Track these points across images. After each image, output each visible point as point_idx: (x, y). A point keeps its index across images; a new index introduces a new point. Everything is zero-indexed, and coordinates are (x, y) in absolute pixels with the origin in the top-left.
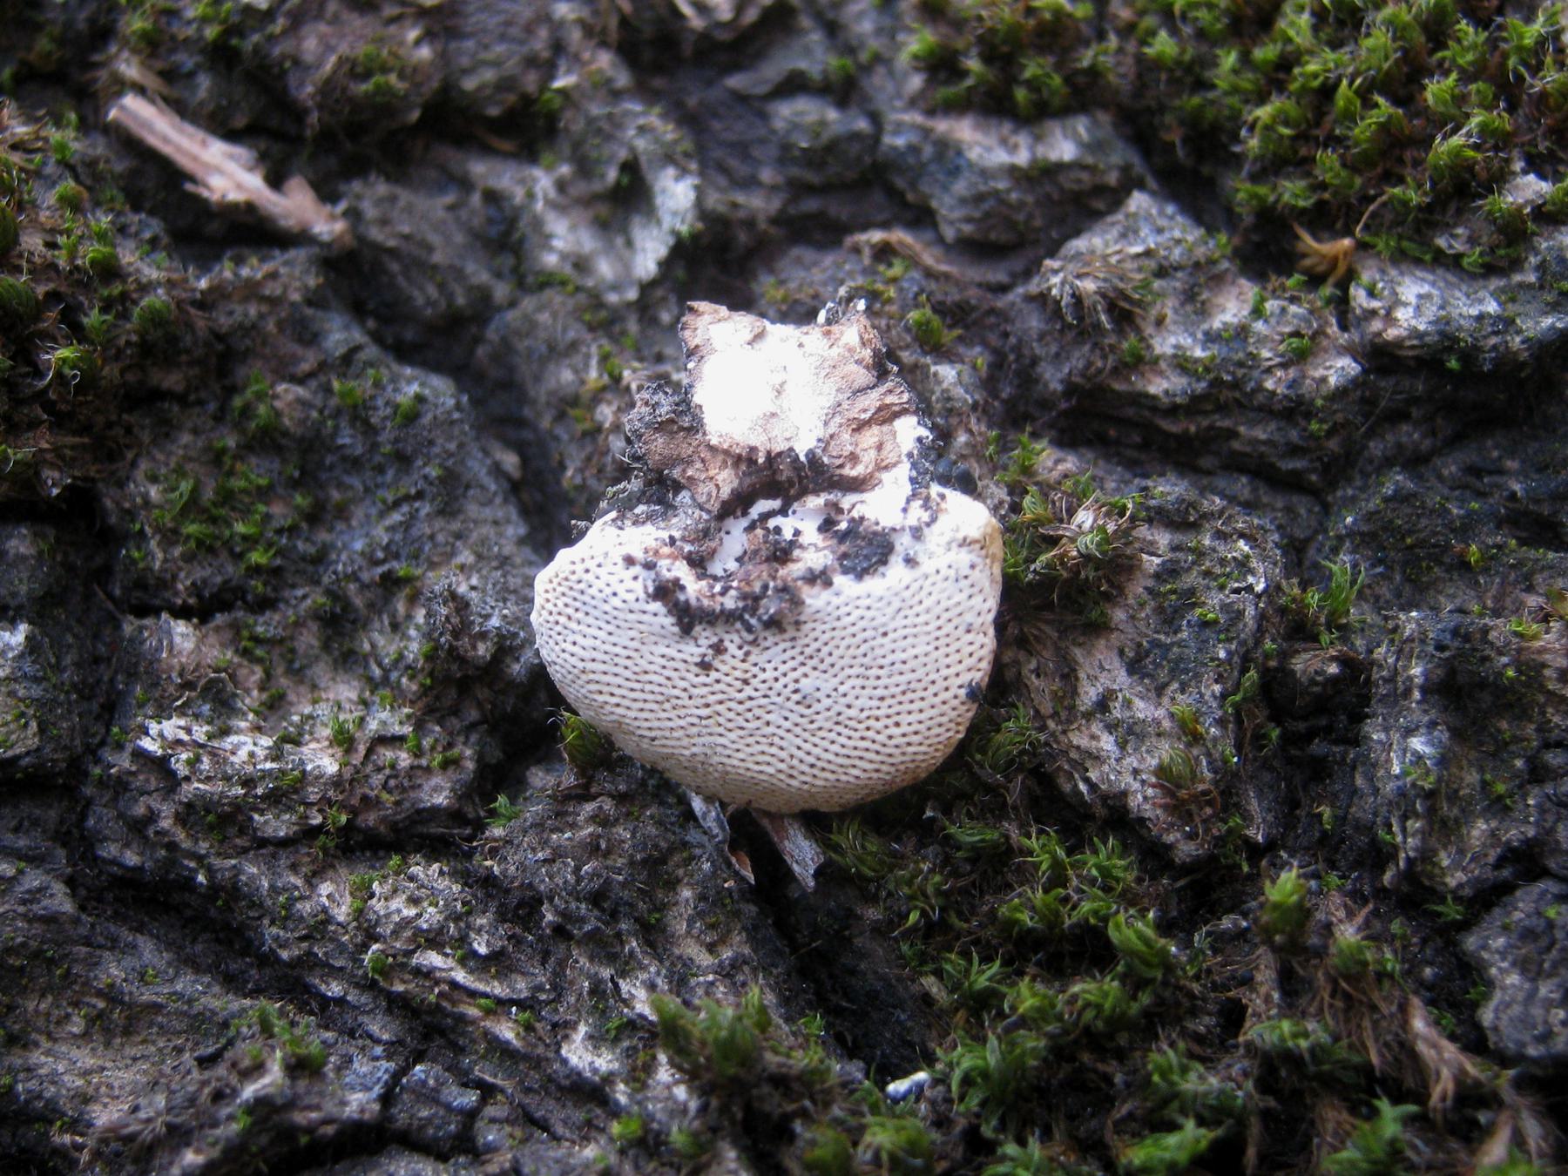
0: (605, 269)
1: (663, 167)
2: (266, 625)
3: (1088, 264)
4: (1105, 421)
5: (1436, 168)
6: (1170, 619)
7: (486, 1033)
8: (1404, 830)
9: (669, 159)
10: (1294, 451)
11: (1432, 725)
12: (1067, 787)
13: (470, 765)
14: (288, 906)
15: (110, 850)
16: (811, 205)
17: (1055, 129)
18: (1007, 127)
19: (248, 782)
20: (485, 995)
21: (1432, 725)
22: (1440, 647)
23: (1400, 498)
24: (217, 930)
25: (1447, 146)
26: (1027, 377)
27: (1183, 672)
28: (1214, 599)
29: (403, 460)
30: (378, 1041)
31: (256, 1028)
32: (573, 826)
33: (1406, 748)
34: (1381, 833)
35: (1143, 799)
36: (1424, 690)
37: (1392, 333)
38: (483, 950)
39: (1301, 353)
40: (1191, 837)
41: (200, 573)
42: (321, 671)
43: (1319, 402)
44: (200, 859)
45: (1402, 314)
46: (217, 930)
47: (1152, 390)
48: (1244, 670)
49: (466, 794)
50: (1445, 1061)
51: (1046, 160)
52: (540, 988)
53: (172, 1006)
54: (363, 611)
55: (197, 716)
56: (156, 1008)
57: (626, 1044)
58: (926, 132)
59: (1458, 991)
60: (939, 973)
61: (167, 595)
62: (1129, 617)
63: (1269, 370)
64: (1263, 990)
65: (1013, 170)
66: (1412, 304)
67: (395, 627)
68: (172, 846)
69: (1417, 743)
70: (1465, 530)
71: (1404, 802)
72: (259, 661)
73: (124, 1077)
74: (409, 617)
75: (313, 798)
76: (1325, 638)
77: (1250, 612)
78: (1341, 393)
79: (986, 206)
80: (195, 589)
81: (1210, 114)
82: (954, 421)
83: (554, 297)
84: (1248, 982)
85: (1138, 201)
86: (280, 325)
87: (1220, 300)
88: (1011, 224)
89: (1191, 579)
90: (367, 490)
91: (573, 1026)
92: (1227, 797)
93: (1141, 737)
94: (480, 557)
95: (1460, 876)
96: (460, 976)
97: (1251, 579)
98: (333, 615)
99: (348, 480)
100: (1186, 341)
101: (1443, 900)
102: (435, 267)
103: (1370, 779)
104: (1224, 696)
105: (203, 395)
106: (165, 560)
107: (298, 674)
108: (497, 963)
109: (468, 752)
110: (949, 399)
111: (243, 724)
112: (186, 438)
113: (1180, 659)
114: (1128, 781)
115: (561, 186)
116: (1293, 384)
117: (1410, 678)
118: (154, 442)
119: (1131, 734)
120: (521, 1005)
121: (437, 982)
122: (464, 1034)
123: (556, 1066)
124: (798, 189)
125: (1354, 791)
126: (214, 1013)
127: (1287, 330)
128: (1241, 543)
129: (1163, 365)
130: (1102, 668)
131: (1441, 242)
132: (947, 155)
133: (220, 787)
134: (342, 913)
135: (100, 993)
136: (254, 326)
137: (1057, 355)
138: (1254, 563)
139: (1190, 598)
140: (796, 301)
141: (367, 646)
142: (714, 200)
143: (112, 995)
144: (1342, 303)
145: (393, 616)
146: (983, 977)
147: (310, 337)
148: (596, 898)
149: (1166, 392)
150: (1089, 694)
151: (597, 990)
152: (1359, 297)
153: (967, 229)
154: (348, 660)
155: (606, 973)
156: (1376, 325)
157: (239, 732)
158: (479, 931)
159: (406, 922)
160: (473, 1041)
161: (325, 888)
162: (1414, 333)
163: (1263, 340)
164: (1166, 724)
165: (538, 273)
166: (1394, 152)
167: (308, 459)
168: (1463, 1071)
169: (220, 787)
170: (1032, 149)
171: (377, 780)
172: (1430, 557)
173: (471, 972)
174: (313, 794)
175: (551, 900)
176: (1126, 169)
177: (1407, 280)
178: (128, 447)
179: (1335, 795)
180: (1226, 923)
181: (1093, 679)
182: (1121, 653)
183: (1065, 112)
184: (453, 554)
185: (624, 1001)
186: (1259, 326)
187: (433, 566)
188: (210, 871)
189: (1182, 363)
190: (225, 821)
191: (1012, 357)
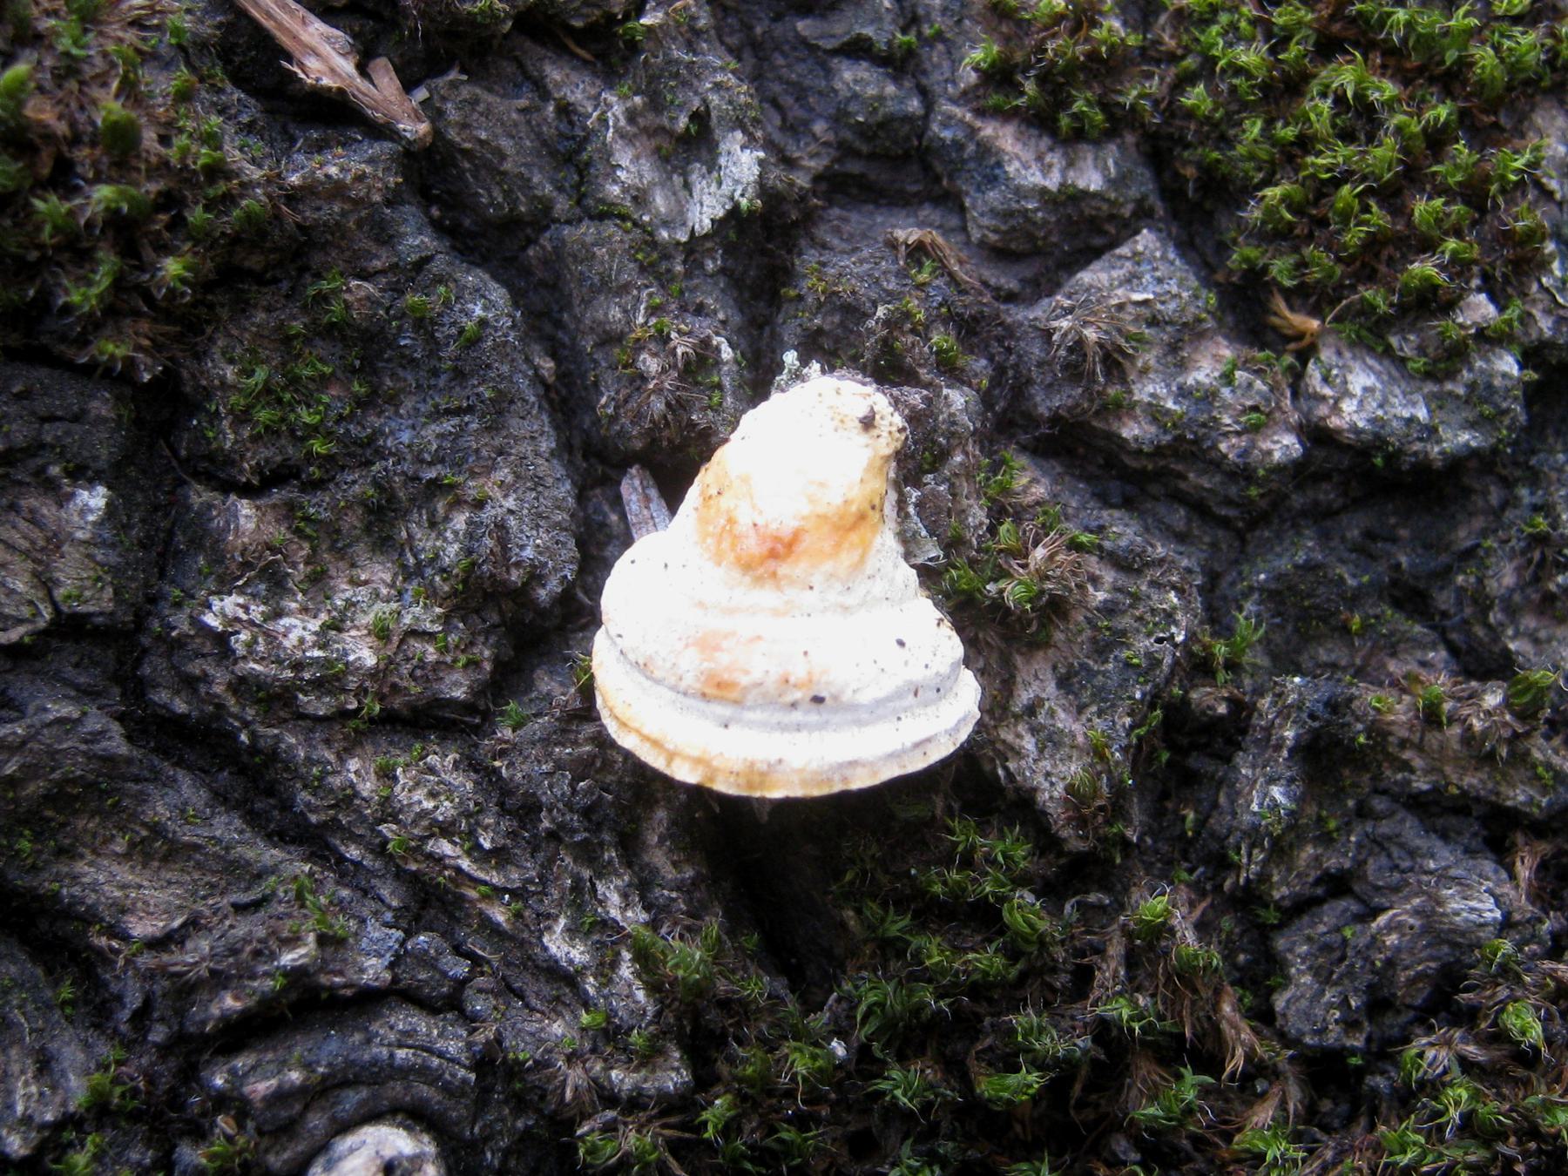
0: (660, 202)
1: (733, 129)
2: (317, 506)
3: (1094, 314)
4: (1081, 448)
5: (1406, 285)
6: (1102, 650)
7: (481, 913)
8: (1250, 855)
9: (739, 124)
10: (1228, 502)
11: (1291, 781)
12: (987, 767)
13: (488, 666)
14: (321, 779)
15: (162, 696)
16: (854, 167)
17: (1087, 154)
18: (1046, 142)
19: (298, 666)
20: (485, 883)
21: (1291, 781)
22: (1312, 716)
23: (1310, 567)
24: (261, 790)
25: (1423, 268)
26: (1020, 390)
27: (1105, 701)
28: (1143, 644)
29: (459, 375)
30: (389, 907)
31: (292, 895)
32: (575, 743)
33: (1265, 794)
34: (1232, 853)
35: (1050, 795)
36: (1291, 751)
37: (1334, 422)
38: (487, 845)
39: (1258, 422)
40: (1085, 838)
41: (264, 453)
42: (361, 550)
43: (1261, 472)
44: (246, 724)
45: (1348, 406)
46: (261, 790)
47: (1125, 433)
48: (1152, 707)
49: (478, 691)
50: (1242, 1040)
51: (1074, 186)
52: (530, 881)
53: (211, 849)
54: (406, 504)
55: (254, 596)
56: (197, 847)
57: (596, 937)
58: (972, 132)
59: (1260, 977)
60: (859, 911)
61: (234, 471)
62: (1071, 640)
63: (1226, 435)
64: (1113, 965)
65: (1044, 191)
66: (1360, 394)
67: (433, 524)
68: (220, 707)
69: (1277, 792)
70: (1354, 600)
71: (1254, 835)
72: (308, 538)
73: (157, 896)
74: (447, 519)
75: (352, 686)
76: (1222, 676)
77: (1168, 660)
78: (1279, 469)
79: (1013, 222)
80: (257, 470)
81: (1224, 169)
82: (954, 442)
83: (610, 229)
84: (1100, 951)
85: (1146, 240)
86: (360, 224)
87: (1197, 356)
88: (1031, 238)
89: (1125, 622)
90: (419, 386)
91: (556, 918)
92: (1117, 809)
93: (1057, 745)
94: (518, 476)
95: (1285, 890)
96: (465, 864)
97: (1173, 629)
98: (380, 507)
99: (401, 373)
100: (1161, 391)
101: (1267, 906)
102: (504, 173)
103: (1232, 802)
104: (1132, 727)
105: (278, 273)
106: (236, 442)
107: (341, 553)
108: (499, 857)
109: (487, 653)
110: (954, 423)
111: (294, 605)
112: (260, 317)
113: (1103, 688)
114: (1039, 780)
115: (632, 116)
116: (1245, 453)
117: (1283, 739)
118: (231, 319)
119: (1051, 741)
120: (515, 894)
121: (446, 867)
122: (461, 908)
123: (537, 950)
124: (845, 150)
125: (1215, 805)
126: (248, 863)
127: (1249, 403)
128: (1172, 594)
129: (1138, 411)
130: (1036, 677)
131: (1394, 341)
132: (989, 164)
133: (273, 670)
134: (367, 787)
135: (144, 825)
136: (337, 223)
137: (1050, 385)
138: (1179, 616)
139: (1120, 638)
140: (836, 293)
141: (404, 534)
142: (776, 175)
143: (157, 830)
144: (1297, 377)
145: (432, 514)
146: (896, 926)
147: (385, 236)
148: (587, 812)
149: (1136, 439)
150: (1024, 696)
151: (577, 888)
152: (1314, 374)
153: (993, 237)
154: (384, 544)
155: (587, 873)
156: (1323, 410)
157: (289, 614)
158: (486, 828)
159: (424, 814)
160: (468, 916)
161: (354, 764)
162: (1354, 429)
163: (1226, 407)
164: (1080, 739)
165: (602, 201)
166: (1372, 260)
167: (368, 350)
168: (1253, 1049)
169: (273, 670)
170: (1063, 172)
171: (405, 669)
172: (1320, 618)
173: (475, 861)
174: (353, 682)
175: (550, 811)
176: (1140, 202)
177: (1357, 366)
178: (208, 322)
179: (1200, 801)
180: (1092, 898)
181: (1027, 684)
182: (1054, 668)
183: (1099, 140)
184: (493, 468)
185: (600, 902)
186: (1226, 392)
187: (473, 475)
188: (254, 736)
189: (1155, 413)
190: (277, 700)
191: (1010, 373)
